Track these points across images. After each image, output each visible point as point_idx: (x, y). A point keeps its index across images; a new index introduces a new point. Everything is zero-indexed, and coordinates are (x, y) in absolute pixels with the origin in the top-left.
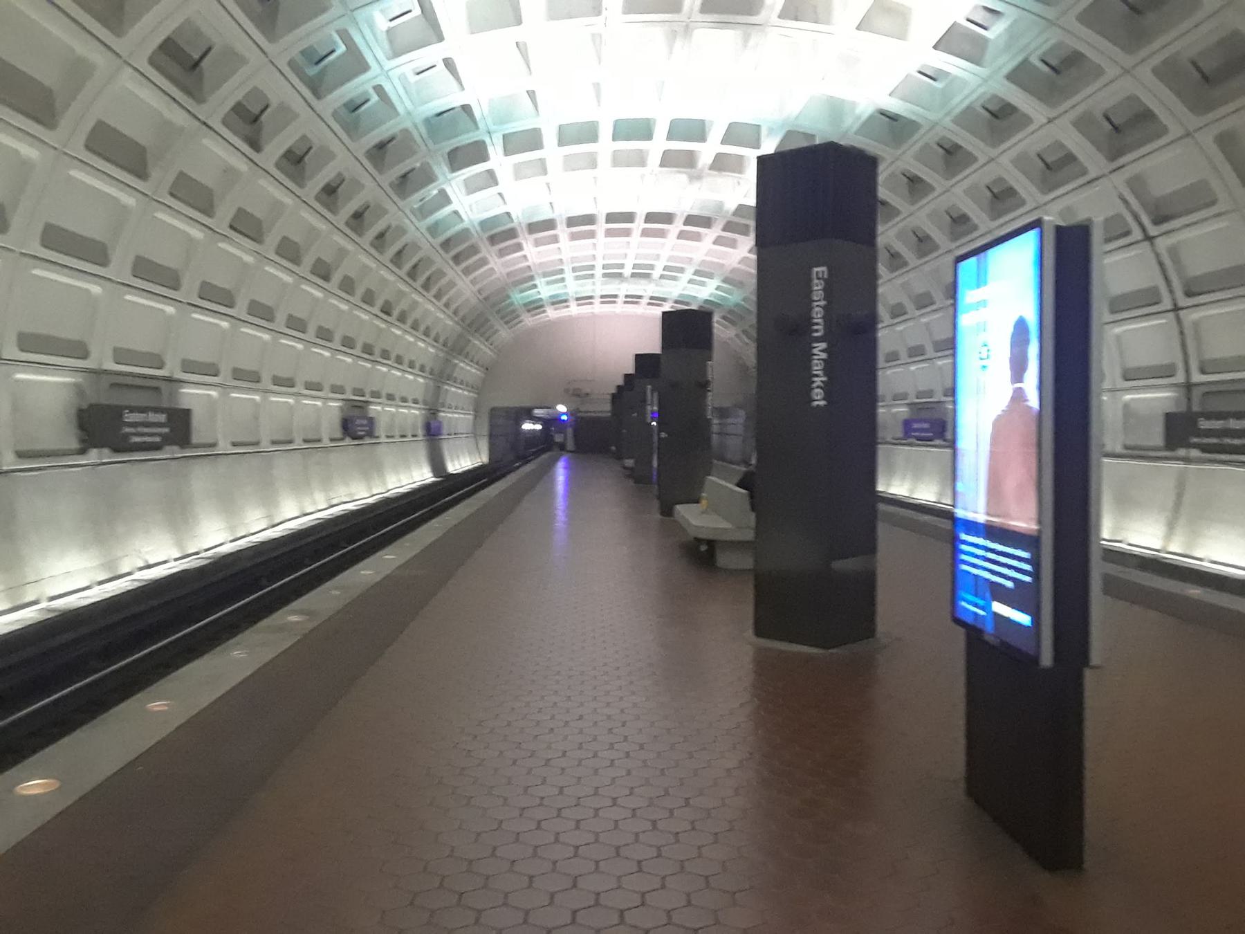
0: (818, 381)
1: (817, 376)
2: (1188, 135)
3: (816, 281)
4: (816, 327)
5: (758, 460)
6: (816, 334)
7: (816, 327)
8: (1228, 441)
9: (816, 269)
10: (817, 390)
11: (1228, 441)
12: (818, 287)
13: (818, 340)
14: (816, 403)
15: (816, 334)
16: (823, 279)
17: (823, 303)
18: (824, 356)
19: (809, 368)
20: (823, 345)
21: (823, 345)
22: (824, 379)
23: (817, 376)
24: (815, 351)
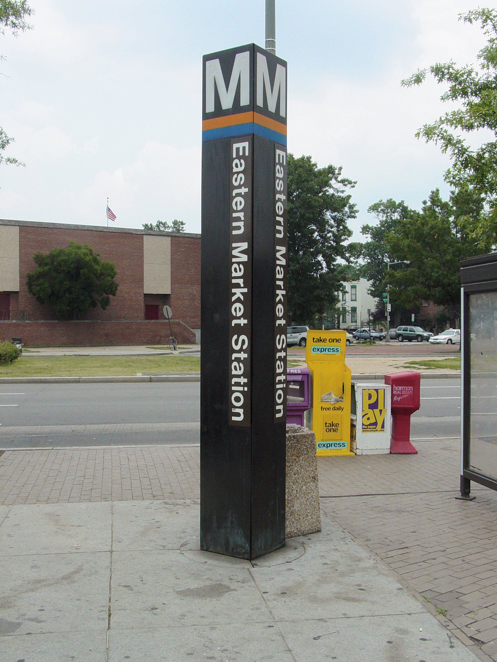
0: (238, 293)
1: (238, 286)
2: (111, 552)
3: (236, 161)
4: (235, 224)
5: (315, 224)
6: (234, 232)
7: (235, 224)
8: (240, 344)
9: (235, 146)
10: (238, 305)
11: (240, 344)
12: (239, 166)
13: (240, 239)
14: (234, 322)
15: (234, 232)
16: (244, 157)
17: (244, 190)
18: (244, 258)
19: (251, 384)
20: (244, 246)
21: (244, 246)
22: (245, 290)
23: (238, 286)
24: (235, 252)
